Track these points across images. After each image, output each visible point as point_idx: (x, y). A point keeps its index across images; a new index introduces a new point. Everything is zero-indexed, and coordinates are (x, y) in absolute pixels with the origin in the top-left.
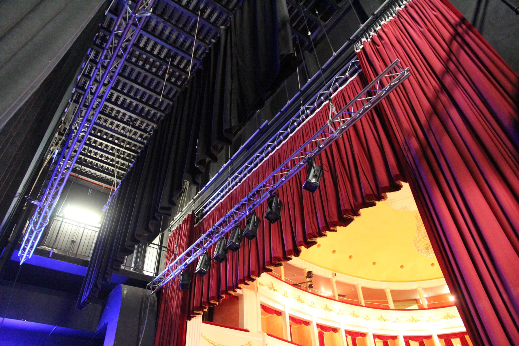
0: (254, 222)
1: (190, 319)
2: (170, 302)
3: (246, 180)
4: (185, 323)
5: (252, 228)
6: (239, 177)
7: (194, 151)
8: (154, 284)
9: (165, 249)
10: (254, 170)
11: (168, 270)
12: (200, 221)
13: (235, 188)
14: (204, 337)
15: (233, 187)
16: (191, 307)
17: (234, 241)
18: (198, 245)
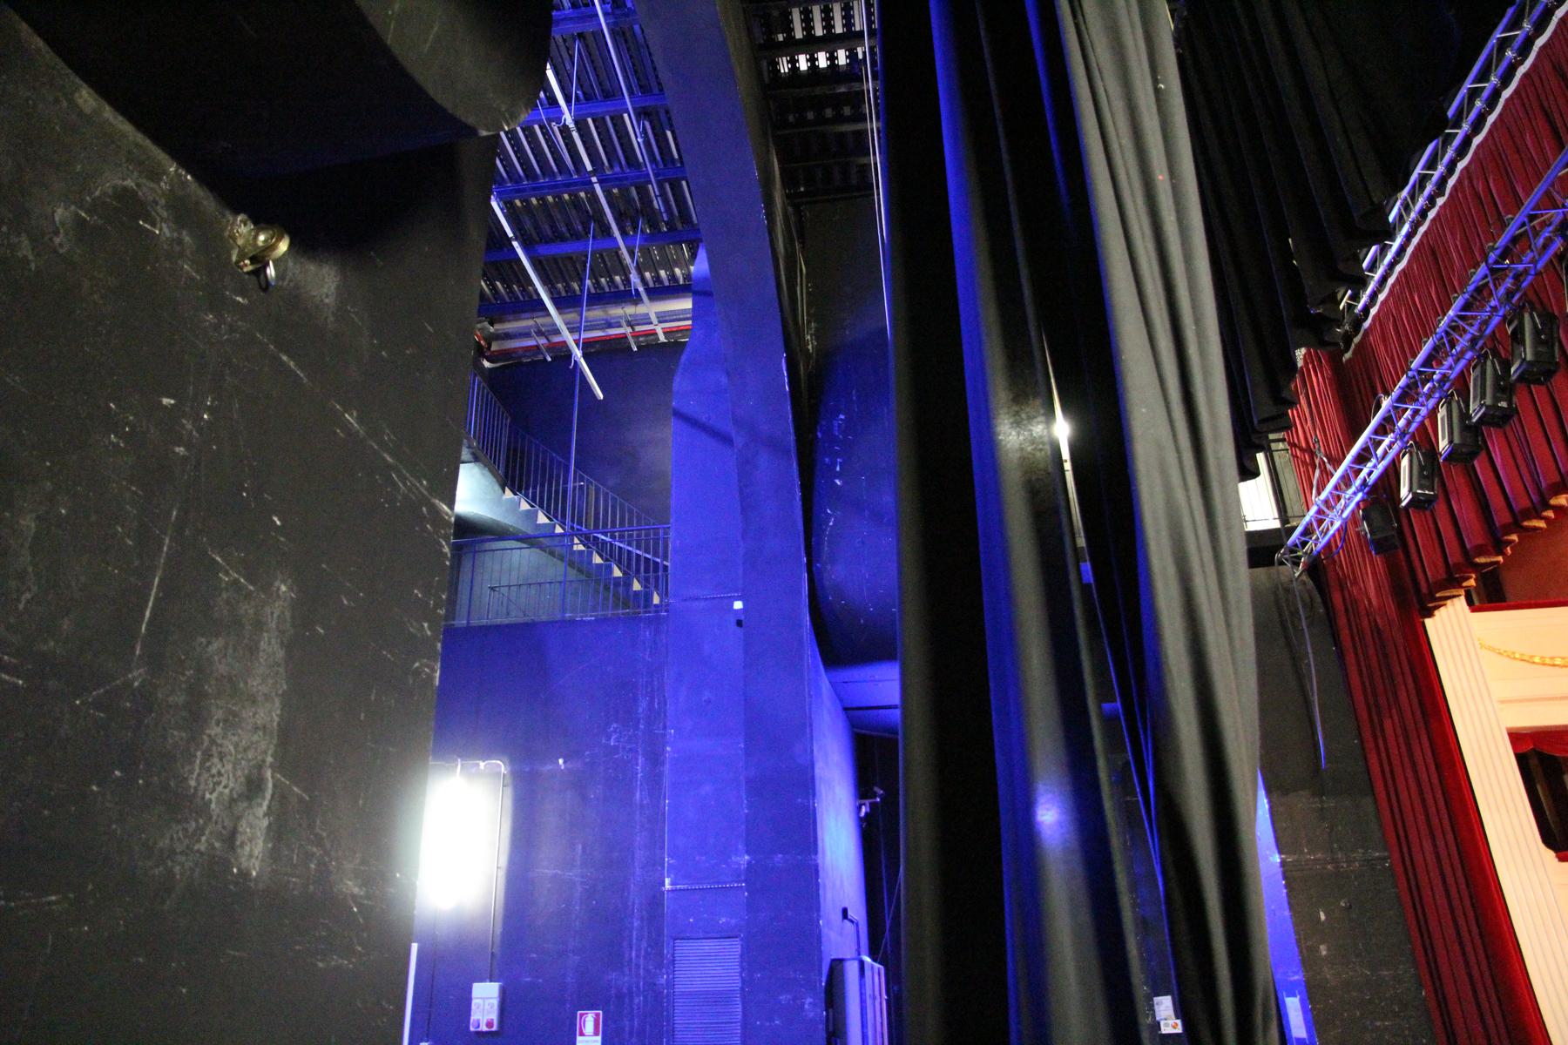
0: (1536, 332)
1: (1430, 614)
2: (1355, 582)
3: (1459, 181)
4: (1420, 630)
5: (1536, 354)
6: (1434, 179)
7: (1294, 276)
8: (1292, 551)
9: (1281, 446)
10: (1477, 140)
11: (1319, 512)
12: (1357, 340)
13: (1432, 214)
14: (1490, 649)
15: (1423, 214)
16: (1423, 584)
17: (1488, 401)
18: (1382, 430)
